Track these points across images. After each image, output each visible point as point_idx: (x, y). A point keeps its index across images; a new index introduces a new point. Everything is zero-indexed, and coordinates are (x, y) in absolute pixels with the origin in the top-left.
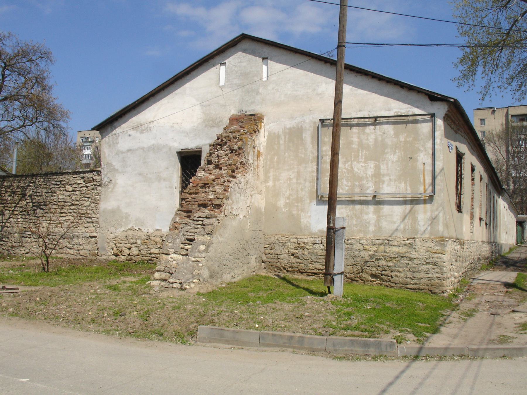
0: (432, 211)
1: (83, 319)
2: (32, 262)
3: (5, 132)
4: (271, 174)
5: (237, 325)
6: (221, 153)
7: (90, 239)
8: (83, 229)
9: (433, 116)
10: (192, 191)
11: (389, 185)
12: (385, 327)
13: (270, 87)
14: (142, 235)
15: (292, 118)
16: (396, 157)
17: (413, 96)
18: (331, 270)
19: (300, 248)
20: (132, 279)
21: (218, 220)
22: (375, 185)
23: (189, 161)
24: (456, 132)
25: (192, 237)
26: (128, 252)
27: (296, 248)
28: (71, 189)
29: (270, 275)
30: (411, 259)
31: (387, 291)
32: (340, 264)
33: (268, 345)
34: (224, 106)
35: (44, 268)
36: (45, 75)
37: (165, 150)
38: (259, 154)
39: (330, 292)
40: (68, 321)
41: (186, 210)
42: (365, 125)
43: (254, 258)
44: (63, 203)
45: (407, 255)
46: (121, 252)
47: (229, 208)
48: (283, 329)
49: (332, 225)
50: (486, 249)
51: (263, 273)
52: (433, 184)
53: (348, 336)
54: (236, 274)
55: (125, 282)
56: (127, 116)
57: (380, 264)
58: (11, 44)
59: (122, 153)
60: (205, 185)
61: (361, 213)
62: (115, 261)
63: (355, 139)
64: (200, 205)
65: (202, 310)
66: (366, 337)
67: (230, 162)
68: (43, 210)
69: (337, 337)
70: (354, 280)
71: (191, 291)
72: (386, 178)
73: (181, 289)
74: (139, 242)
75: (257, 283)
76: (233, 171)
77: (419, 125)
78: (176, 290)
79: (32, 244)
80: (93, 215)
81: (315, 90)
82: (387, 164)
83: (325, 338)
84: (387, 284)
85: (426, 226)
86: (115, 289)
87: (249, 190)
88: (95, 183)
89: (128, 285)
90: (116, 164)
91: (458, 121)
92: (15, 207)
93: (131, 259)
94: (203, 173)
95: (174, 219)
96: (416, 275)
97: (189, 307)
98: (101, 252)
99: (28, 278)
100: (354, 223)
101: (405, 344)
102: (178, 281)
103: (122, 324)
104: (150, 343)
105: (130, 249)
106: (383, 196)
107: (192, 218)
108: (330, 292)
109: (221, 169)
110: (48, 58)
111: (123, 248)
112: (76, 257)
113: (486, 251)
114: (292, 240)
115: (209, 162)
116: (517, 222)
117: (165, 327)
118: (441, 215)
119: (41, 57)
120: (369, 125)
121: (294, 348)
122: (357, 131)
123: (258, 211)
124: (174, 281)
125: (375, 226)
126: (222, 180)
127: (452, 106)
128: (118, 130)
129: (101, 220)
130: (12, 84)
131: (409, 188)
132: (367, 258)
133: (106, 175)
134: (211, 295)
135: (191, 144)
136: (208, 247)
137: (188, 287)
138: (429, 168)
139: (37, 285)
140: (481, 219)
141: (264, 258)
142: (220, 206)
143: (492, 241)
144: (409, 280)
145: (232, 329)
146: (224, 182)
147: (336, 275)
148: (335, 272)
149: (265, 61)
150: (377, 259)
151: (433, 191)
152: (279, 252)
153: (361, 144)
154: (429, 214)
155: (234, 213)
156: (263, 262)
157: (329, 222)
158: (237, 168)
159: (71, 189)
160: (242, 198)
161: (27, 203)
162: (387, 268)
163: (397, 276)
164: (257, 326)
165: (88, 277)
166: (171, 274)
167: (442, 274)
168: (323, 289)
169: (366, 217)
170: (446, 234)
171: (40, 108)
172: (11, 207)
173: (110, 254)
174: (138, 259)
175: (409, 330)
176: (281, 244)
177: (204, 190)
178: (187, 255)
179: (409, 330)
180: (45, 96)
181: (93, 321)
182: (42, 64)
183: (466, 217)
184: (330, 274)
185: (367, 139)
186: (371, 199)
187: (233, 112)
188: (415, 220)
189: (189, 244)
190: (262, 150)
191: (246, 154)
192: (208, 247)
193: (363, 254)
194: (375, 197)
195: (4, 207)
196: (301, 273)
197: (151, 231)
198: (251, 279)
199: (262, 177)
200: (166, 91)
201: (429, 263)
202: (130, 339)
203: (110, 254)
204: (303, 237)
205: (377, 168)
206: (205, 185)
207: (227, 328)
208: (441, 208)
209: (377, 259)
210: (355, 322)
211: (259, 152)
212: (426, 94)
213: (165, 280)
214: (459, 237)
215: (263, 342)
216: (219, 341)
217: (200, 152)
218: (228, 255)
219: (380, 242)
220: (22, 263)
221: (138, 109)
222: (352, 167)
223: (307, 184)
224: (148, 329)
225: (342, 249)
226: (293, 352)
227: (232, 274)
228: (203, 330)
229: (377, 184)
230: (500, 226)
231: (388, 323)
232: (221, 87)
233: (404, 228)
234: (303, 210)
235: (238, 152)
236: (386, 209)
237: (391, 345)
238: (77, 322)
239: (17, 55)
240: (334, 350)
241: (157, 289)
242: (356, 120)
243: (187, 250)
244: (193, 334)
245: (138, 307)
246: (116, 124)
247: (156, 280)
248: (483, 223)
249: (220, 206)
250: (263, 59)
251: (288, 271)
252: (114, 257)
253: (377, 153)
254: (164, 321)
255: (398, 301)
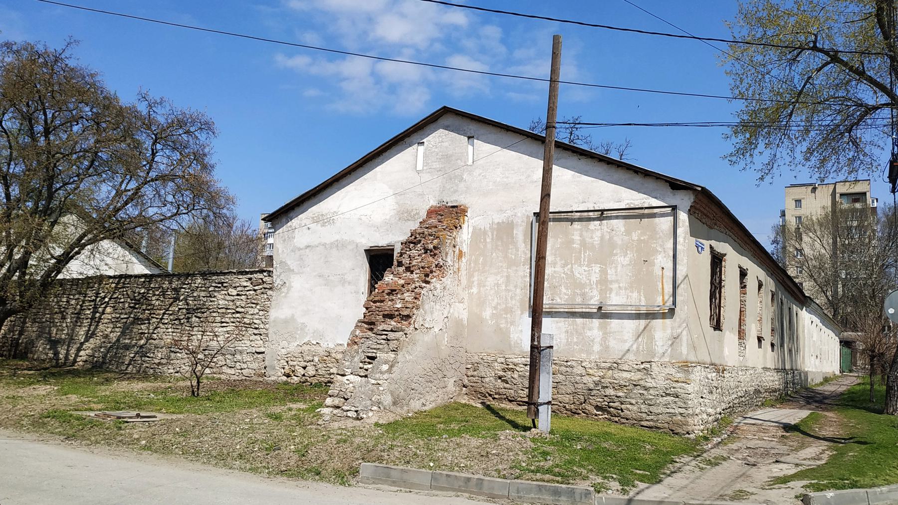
0: (672, 328)
1: (228, 454)
2: (181, 384)
3: (154, 222)
4: (476, 278)
5: (408, 462)
6: (414, 252)
7: (256, 355)
8: (248, 343)
9: (674, 208)
10: (376, 299)
11: (617, 294)
12: (584, 472)
13: (476, 173)
14: (321, 351)
15: (501, 211)
16: (627, 259)
17: (650, 184)
18: (535, 398)
19: (509, 369)
20: (301, 405)
21: (406, 334)
22: (600, 294)
23: (380, 260)
24: (711, 228)
25: (374, 355)
26: (302, 371)
27: (504, 370)
28: (234, 292)
29: (472, 403)
30: (646, 389)
31: (613, 429)
32: (545, 393)
33: (442, 489)
34: (422, 195)
35: (193, 392)
36: (206, 150)
37: (350, 247)
38: (461, 254)
39: (535, 427)
40: (208, 454)
41: (369, 323)
42: (590, 219)
43: (452, 380)
44: (224, 310)
45: (642, 383)
46: (293, 371)
47: (420, 320)
48: (461, 469)
49: (536, 343)
50: (772, 378)
51: (464, 400)
52: (674, 295)
53: (537, 480)
54: (428, 401)
55: (290, 409)
56: (306, 205)
57: (607, 393)
58: (163, 111)
59: (300, 249)
60: (392, 292)
61: (584, 328)
62: (286, 383)
63: (577, 237)
64: (385, 316)
65: (371, 443)
66: (558, 482)
67: (423, 264)
68: (200, 318)
69: (523, 481)
70: (575, 413)
71: (368, 421)
72: (615, 286)
73: (357, 419)
74: (316, 359)
75: (452, 413)
76: (427, 275)
77: (657, 220)
78: (351, 420)
79: (182, 361)
80: (262, 326)
81: (529, 176)
82: (616, 267)
83: (509, 481)
84: (617, 419)
85: (665, 348)
86: (276, 418)
87: (447, 298)
88: (265, 286)
89: (293, 413)
90: (292, 263)
91: (711, 214)
92: (164, 314)
93: (306, 381)
94: (391, 276)
95: (353, 332)
96: (654, 409)
97: (358, 440)
98: (269, 372)
99: (175, 404)
100: (575, 340)
101: (604, 494)
102: (353, 409)
103: (274, 461)
104: (303, 483)
105: (304, 368)
106: (611, 308)
107: (375, 330)
108: (535, 427)
109: (412, 272)
110: (210, 129)
111: (297, 367)
112: (237, 378)
113: (773, 380)
114: (499, 360)
115: (400, 264)
116: (841, 342)
117: (324, 465)
118: (685, 333)
119: (201, 128)
120: (594, 219)
121: (471, 492)
122: (579, 227)
123: (459, 323)
124: (348, 408)
125: (601, 345)
126: (413, 286)
127: (700, 197)
128: (295, 222)
129: (270, 332)
130: (165, 161)
131: (643, 299)
132: (592, 386)
133: (279, 276)
134: (392, 427)
135: (381, 241)
136: (391, 367)
137: (364, 416)
138: (669, 273)
139: (181, 413)
140: (760, 339)
141: (466, 382)
142: (408, 317)
143: (788, 367)
144: (644, 415)
145: (402, 467)
146: (416, 288)
147: (541, 404)
148: (540, 401)
149: (471, 140)
150: (603, 387)
151: (674, 303)
152: (483, 374)
153: (583, 244)
154: (669, 331)
155: (427, 325)
156: (464, 386)
157: (533, 340)
158: (432, 272)
159: (234, 292)
160: (438, 307)
161: (180, 309)
162: (616, 399)
163: (628, 409)
164: (432, 464)
165: (246, 403)
166: (346, 399)
167: (686, 408)
168: (529, 423)
169: (589, 333)
170: (692, 358)
171: (200, 191)
172: (159, 314)
173: (280, 374)
174: (314, 381)
175: (615, 476)
176: (486, 365)
177: (392, 297)
178: (366, 376)
179: (615, 476)
180: (205, 177)
181: (241, 456)
182: (202, 136)
183: (730, 335)
184: (534, 404)
185: (592, 238)
186: (595, 311)
187: (433, 202)
188: (652, 338)
189: (370, 363)
190: (465, 249)
191: (444, 255)
192: (391, 367)
193: (586, 379)
194: (600, 308)
195: (150, 314)
196: (511, 401)
197: (331, 346)
198: (446, 407)
199: (464, 281)
200: (354, 175)
201: (669, 395)
202: (280, 479)
203: (280, 374)
204: (512, 356)
205: (603, 272)
206: (392, 292)
207: (395, 467)
208: (685, 325)
209: (603, 387)
210: (548, 464)
211: (461, 252)
212: (667, 181)
213: (338, 407)
214: (717, 362)
215: (436, 485)
216: (384, 482)
217: (393, 250)
218: (417, 377)
219: (608, 365)
220: (168, 385)
221: (319, 196)
222: (572, 272)
223: (518, 291)
224: (306, 469)
225: (548, 373)
226: (470, 498)
227: (423, 400)
228: (367, 468)
229: (601, 292)
230: (804, 347)
231: (590, 467)
232: (418, 172)
233: (638, 348)
234: (512, 323)
235: (433, 252)
236: (614, 323)
237: (587, 494)
238: (222, 459)
239: (170, 125)
240: (518, 497)
241: (328, 418)
242: (578, 214)
243: (367, 370)
244: (355, 472)
245: (297, 440)
246: (291, 214)
247: (328, 407)
248: (766, 344)
249: (408, 317)
250: (469, 138)
251: (494, 398)
252: (285, 378)
253: (604, 255)
254: (325, 457)
255: (620, 442)
